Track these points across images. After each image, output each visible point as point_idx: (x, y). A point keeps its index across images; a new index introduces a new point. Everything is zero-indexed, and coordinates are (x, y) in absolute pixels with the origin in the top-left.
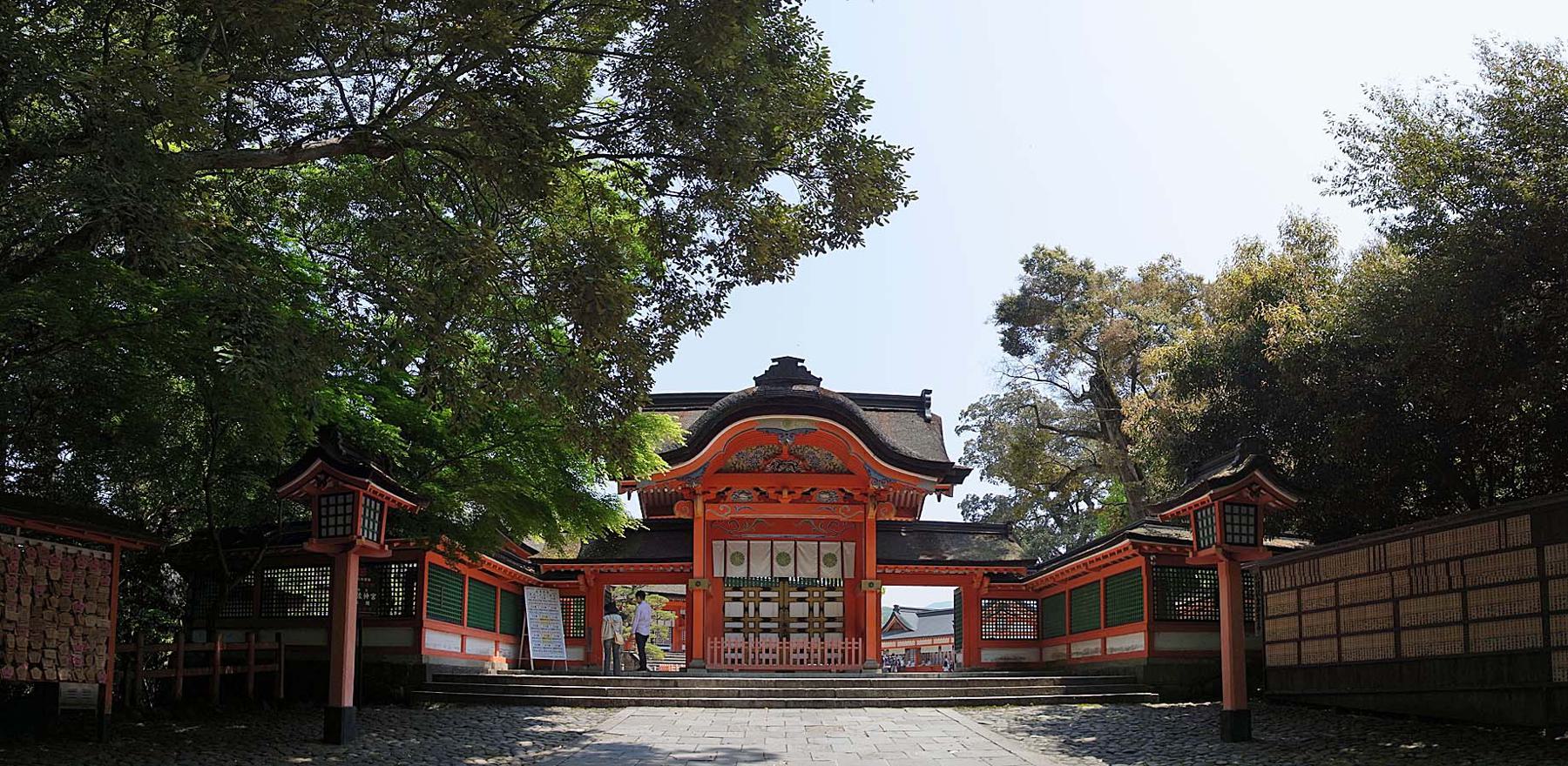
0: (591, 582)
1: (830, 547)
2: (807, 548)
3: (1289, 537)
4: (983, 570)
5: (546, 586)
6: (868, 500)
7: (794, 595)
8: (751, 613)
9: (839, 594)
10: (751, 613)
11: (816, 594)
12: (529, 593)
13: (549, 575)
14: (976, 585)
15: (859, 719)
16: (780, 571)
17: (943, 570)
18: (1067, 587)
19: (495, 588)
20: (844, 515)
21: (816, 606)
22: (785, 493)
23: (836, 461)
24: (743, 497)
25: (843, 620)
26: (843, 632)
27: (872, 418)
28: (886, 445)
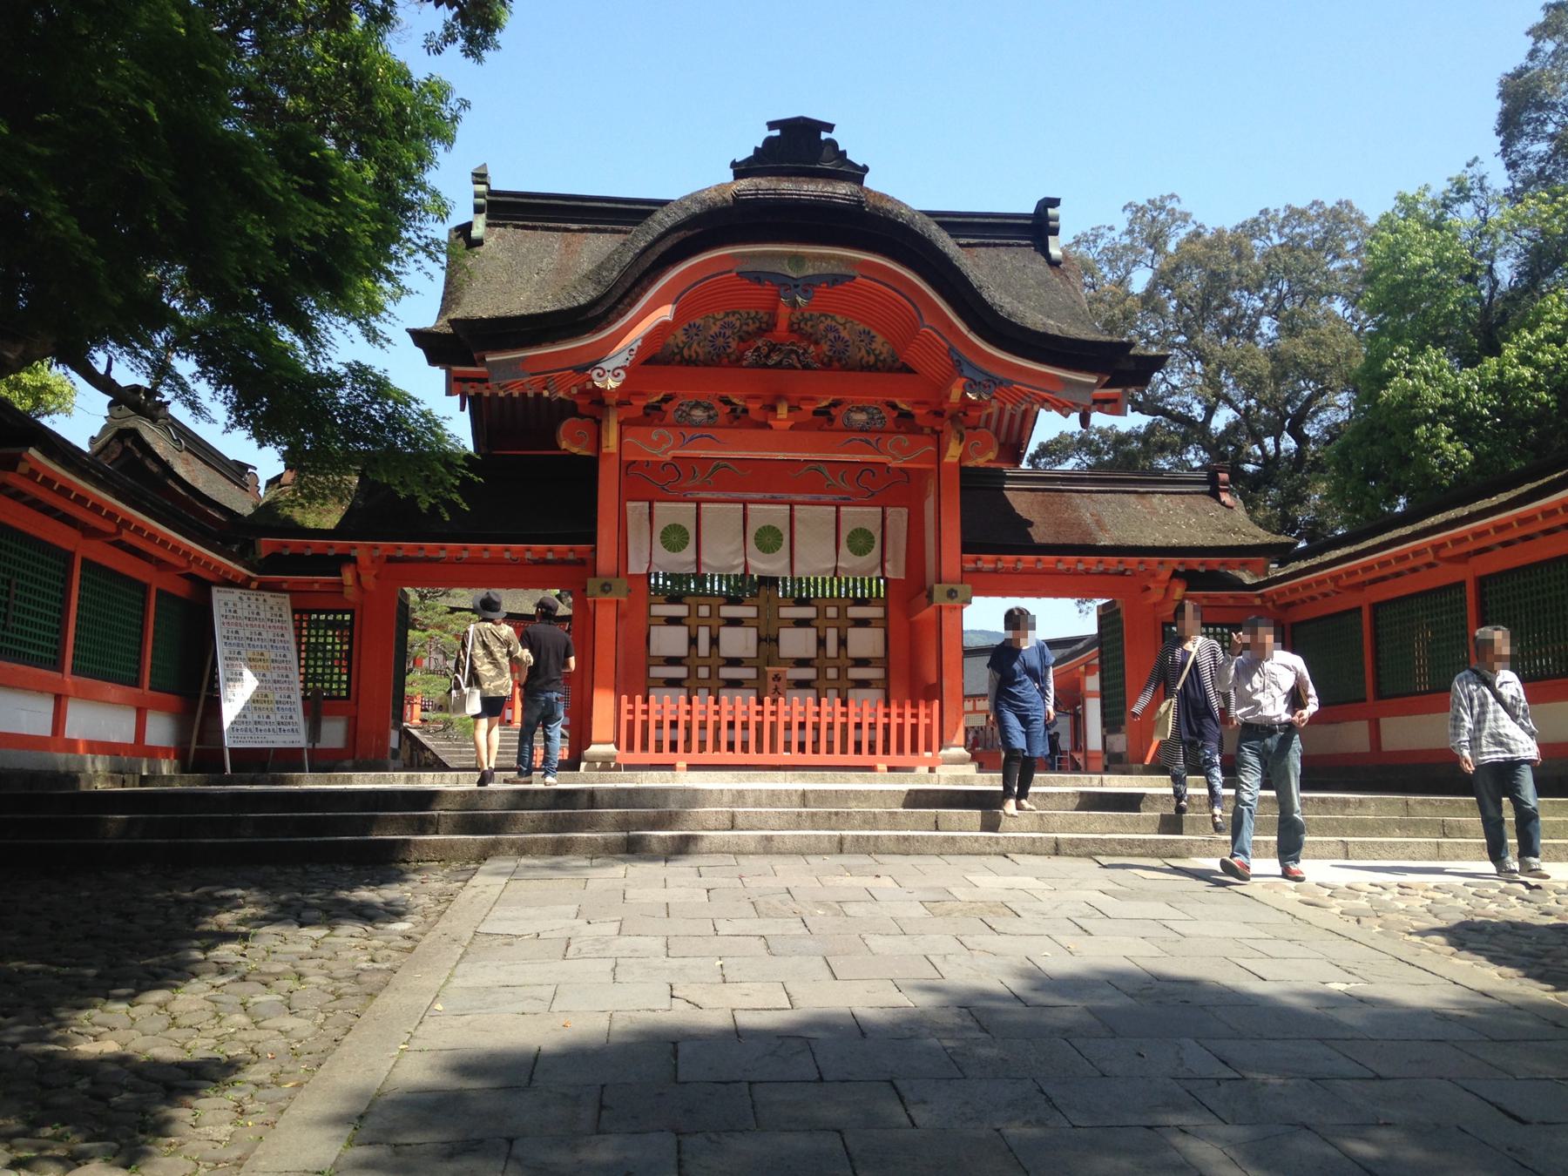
0: (368, 579)
2: (815, 519)
5: (263, 587)
7: (789, 612)
8: (832, 649)
9: (874, 612)
10: (832, 649)
11: (704, 611)
12: (221, 600)
13: (276, 563)
14: (1157, 594)
15: (675, 895)
16: (762, 565)
17: (1028, 560)
19: (144, 588)
20: (895, 455)
21: (704, 635)
22: (783, 411)
24: (698, 414)
25: (885, 662)
26: (886, 686)
28: (1045, 337)
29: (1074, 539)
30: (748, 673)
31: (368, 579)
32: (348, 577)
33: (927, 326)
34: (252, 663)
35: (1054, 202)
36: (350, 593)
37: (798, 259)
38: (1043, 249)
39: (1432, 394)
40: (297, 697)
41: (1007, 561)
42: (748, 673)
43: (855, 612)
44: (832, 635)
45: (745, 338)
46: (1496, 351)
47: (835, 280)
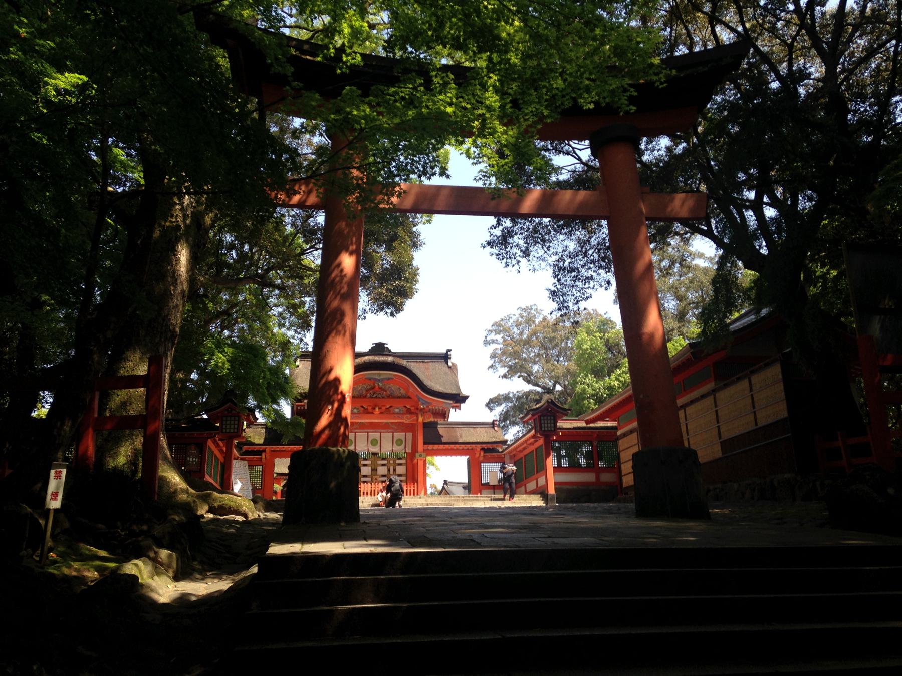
0: (268, 456)
1: (400, 435)
2: (387, 436)
3: (92, 400)
4: (479, 447)
5: (242, 459)
6: (418, 411)
9: (403, 461)
13: (247, 453)
14: (477, 455)
16: (375, 449)
17: (441, 447)
18: (522, 455)
20: (407, 419)
22: (377, 409)
23: (402, 391)
25: (406, 475)
27: (416, 367)
29: (453, 440)
30: (369, 479)
31: (268, 456)
32: (263, 456)
33: (411, 389)
34: (239, 479)
35: (450, 350)
36: (263, 460)
37: (380, 374)
38: (447, 363)
39: (589, 390)
40: (250, 488)
41: (436, 447)
42: (369, 479)
43: (398, 462)
44: (392, 468)
45: (367, 390)
46: (609, 375)
47: (389, 379)
